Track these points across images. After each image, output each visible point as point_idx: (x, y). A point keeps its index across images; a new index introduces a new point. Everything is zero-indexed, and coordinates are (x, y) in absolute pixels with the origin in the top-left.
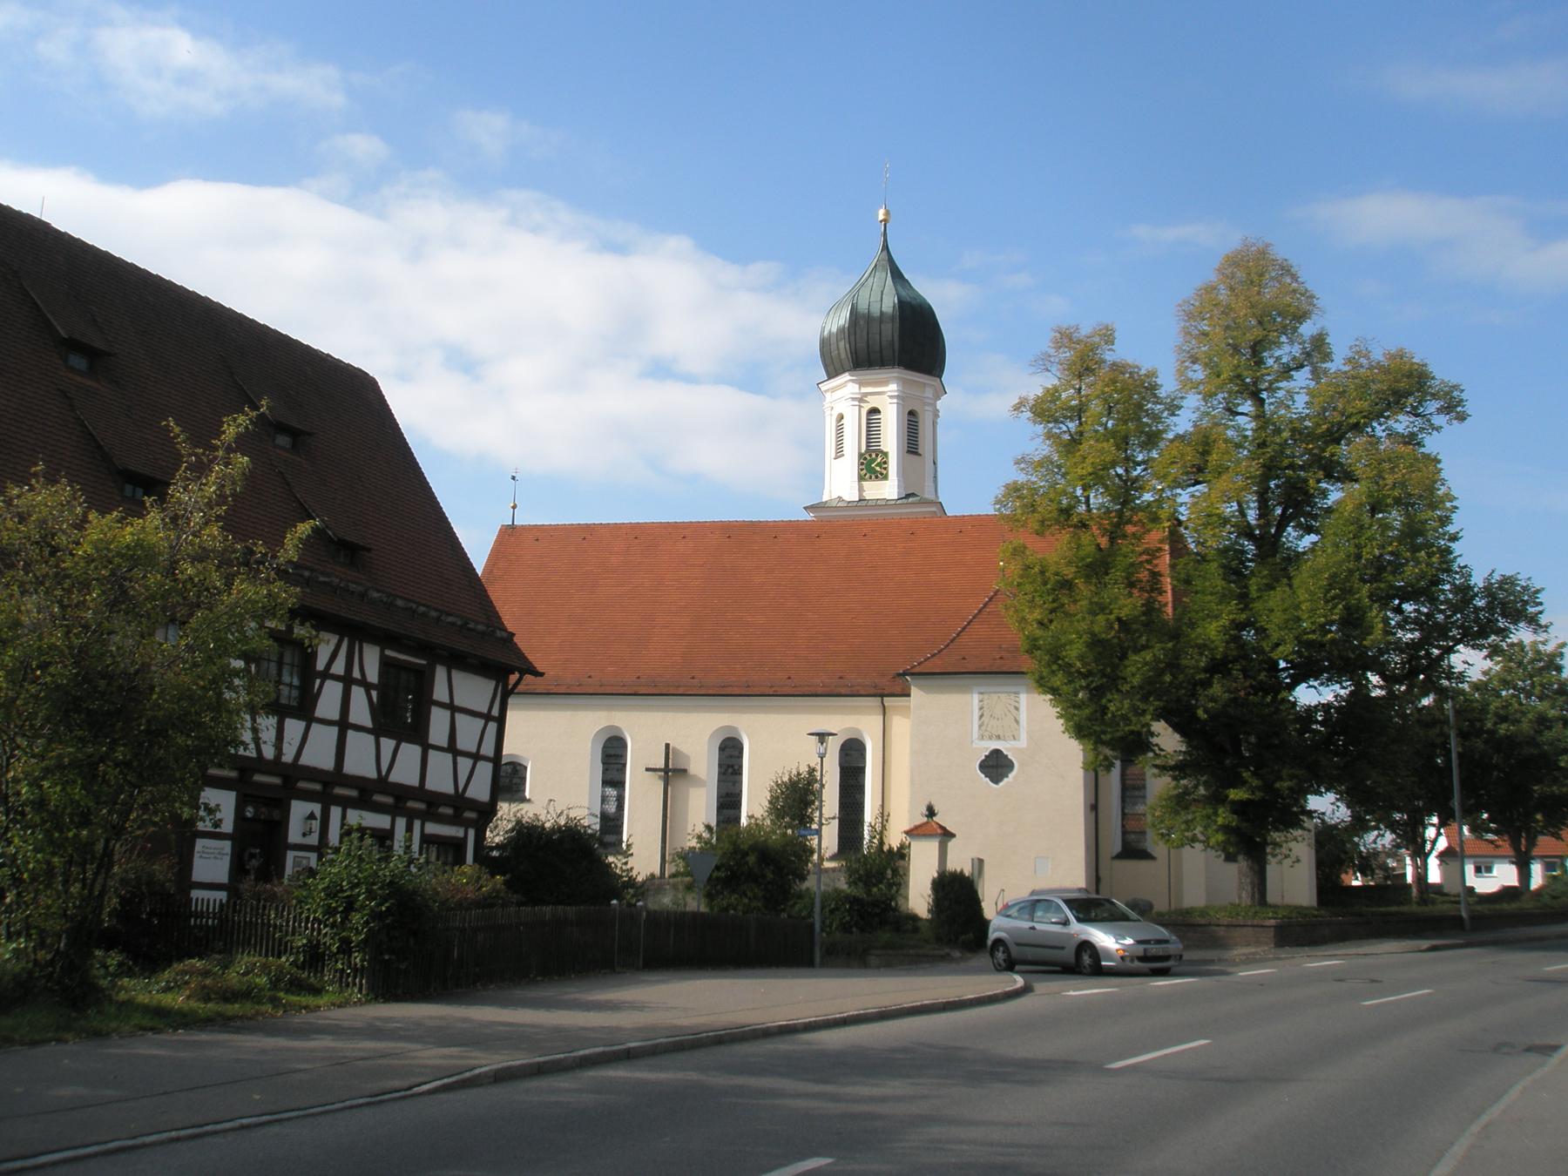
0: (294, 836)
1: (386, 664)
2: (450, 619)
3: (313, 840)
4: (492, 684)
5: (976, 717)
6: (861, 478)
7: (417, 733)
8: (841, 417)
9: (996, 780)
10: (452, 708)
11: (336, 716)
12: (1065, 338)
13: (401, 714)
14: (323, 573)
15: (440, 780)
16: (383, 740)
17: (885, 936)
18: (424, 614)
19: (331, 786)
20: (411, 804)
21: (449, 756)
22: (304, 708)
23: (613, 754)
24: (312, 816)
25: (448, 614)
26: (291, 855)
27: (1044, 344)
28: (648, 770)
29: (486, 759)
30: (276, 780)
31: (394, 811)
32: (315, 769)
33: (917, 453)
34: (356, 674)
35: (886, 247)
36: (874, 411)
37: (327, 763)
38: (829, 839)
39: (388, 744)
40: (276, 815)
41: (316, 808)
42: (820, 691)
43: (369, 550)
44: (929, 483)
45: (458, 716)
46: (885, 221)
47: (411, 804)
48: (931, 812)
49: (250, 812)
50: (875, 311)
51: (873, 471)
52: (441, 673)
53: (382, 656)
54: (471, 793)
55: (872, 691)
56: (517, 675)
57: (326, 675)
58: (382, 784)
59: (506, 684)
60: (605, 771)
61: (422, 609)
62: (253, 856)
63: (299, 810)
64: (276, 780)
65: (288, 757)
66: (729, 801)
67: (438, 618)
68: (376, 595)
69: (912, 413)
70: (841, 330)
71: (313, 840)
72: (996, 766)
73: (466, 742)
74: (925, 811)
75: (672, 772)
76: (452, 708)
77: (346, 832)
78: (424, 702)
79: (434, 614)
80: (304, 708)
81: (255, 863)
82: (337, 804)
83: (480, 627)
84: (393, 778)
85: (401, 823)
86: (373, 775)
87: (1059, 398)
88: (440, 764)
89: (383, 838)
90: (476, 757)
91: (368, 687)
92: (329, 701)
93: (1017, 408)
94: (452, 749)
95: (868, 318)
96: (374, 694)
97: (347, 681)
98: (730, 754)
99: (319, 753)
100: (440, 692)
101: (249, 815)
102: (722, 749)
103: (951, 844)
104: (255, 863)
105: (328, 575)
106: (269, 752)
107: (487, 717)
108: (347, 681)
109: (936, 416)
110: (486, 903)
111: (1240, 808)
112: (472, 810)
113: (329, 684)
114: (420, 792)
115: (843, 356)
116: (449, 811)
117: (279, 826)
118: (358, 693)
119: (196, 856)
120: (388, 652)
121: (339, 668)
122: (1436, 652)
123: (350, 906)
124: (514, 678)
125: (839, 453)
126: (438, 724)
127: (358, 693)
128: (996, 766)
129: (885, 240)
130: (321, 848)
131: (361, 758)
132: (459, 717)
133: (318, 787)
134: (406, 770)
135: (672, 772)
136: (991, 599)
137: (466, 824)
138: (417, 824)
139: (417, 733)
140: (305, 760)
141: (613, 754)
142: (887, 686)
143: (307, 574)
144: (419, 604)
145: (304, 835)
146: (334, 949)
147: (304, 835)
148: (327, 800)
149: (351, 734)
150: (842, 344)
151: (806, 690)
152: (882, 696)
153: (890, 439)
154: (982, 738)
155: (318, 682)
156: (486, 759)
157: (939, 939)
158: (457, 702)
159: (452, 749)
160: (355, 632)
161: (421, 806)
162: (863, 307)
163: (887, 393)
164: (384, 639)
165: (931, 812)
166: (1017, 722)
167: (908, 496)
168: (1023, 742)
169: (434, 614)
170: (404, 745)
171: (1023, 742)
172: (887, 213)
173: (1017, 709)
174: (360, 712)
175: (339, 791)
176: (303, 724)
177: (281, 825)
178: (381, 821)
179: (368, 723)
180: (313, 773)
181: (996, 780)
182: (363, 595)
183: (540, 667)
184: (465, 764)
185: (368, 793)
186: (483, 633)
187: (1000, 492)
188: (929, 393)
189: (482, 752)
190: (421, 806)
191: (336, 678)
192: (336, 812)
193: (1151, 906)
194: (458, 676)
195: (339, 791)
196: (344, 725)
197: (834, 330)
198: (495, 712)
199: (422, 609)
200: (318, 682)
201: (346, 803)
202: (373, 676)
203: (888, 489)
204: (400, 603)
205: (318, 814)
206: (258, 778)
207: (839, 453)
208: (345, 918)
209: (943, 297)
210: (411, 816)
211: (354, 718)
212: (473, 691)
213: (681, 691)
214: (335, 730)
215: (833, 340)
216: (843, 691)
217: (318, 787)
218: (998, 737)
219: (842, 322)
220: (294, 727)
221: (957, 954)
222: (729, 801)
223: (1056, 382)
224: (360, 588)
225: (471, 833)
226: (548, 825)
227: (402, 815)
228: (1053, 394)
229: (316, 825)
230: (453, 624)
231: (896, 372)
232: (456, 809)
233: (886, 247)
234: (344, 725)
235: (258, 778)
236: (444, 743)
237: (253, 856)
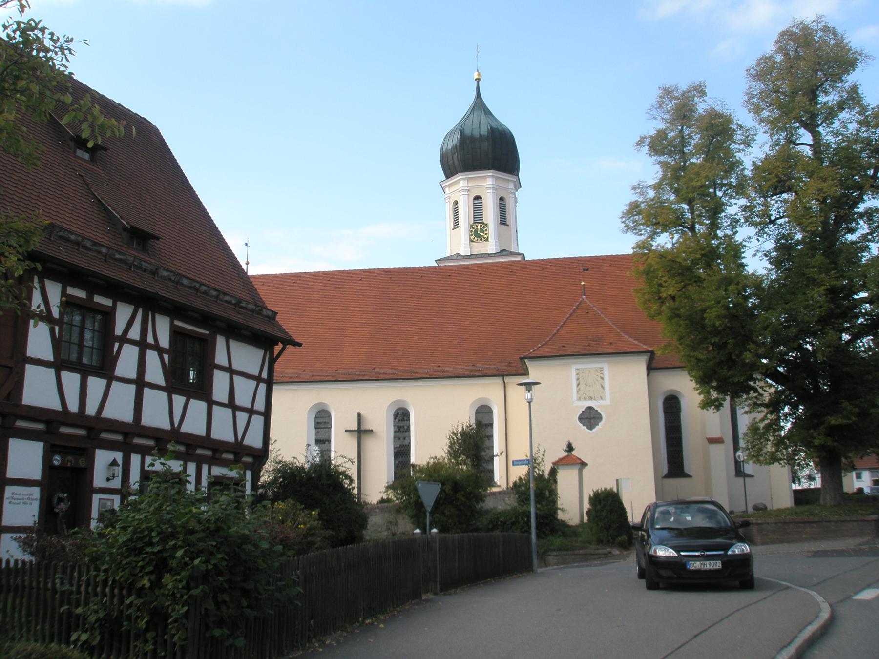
0: (99, 480)
1: (176, 334)
2: (227, 298)
3: (116, 484)
4: (262, 352)
5: (575, 383)
6: (472, 241)
7: (202, 390)
8: (456, 203)
9: (591, 428)
10: (231, 371)
11: (133, 375)
12: (667, 93)
13: (189, 372)
14: (119, 252)
15: (222, 431)
16: (175, 397)
17: (557, 541)
18: (205, 293)
19: (130, 437)
20: (199, 451)
21: (230, 411)
22: (105, 368)
23: (322, 420)
24: (114, 463)
25: (225, 294)
26: (96, 498)
27: (653, 96)
28: (346, 431)
29: (258, 413)
30: (82, 432)
31: (185, 457)
32: (116, 421)
33: (505, 224)
34: (150, 340)
35: (479, 95)
36: (478, 198)
37: (127, 416)
38: (248, 491)
39: (179, 400)
40: (82, 463)
41: (118, 456)
42: (461, 374)
43: (158, 238)
44: (514, 243)
45: (235, 377)
46: (478, 80)
47: (199, 451)
48: (570, 448)
49: (57, 460)
50: (476, 134)
51: (479, 236)
52: (220, 342)
53: (172, 325)
54: (247, 441)
55: (496, 373)
56: (280, 346)
57: (124, 339)
58: (175, 434)
59: (272, 353)
60: (317, 433)
61: (205, 288)
62: (61, 500)
63: (103, 458)
64: (82, 432)
65: (91, 410)
66: (402, 453)
67: (217, 297)
68: (165, 274)
69: (501, 199)
70: (454, 148)
71: (116, 484)
72: (590, 418)
73: (243, 398)
74: (565, 447)
75: (361, 432)
76: (231, 371)
77: (146, 476)
78: (206, 368)
79: (214, 293)
80: (105, 368)
81: (63, 506)
82: (136, 452)
83: (250, 306)
84: (184, 429)
85: (192, 468)
86: (168, 427)
87: (666, 138)
88: (222, 415)
89: (179, 480)
90: (251, 411)
91: (160, 351)
92: (127, 362)
93: (640, 143)
94: (231, 404)
95: (472, 139)
96: (166, 357)
97: (143, 345)
98: (402, 417)
99: (120, 407)
100: (221, 358)
101: (56, 463)
102: (396, 415)
103: (585, 470)
104: (63, 506)
105: (123, 254)
106: (73, 406)
107: (258, 379)
108: (142, 346)
109: (516, 202)
110: (305, 545)
111: (832, 431)
112: (248, 455)
113: (126, 347)
114: (206, 441)
115: (456, 163)
116: (231, 457)
117: (85, 472)
118: (152, 357)
119: (6, 502)
120: (177, 323)
121: (135, 333)
122: (846, 337)
123: (161, 565)
124: (278, 348)
125: (456, 225)
126: (220, 383)
127: (152, 357)
128: (590, 418)
129: (478, 88)
130: (123, 492)
131: (157, 412)
132: (236, 378)
133: (119, 438)
134: (194, 421)
135: (361, 432)
136: (577, 307)
137: (247, 466)
138: (205, 468)
139: (202, 390)
140: (107, 413)
141: (322, 420)
142: (510, 366)
143: (104, 251)
144: (202, 284)
145: (108, 480)
146: (142, 624)
147: (108, 480)
148: (127, 449)
149: (147, 391)
150: (455, 156)
151: (451, 374)
152: (503, 376)
153: (490, 214)
154: (579, 399)
155: (117, 345)
156: (258, 413)
157: (600, 541)
158: (235, 366)
159: (231, 404)
160: (149, 303)
161: (208, 453)
162: (468, 132)
163: (487, 183)
164: (174, 310)
165: (570, 448)
166: (603, 387)
167: (502, 251)
168: (607, 401)
169: (214, 293)
170: (193, 402)
171: (607, 401)
172: (479, 74)
173: (602, 378)
174: (155, 372)
175: (138, 441)
176: (103, 382)
177: (88, 471)
178: (176, 466)
179: (162, 383)
180: (114, 426)
181: (591, 428)
182: (154, 273)
183: (297, 340)
184: (242, 417)
185: (165, 441)
186: (253, 311)
187: (625, 209)
188: (511, 186)
189: (256, 407)
190: (208, 453)
191: (132, 342)
192: (135, 459)
193: (766, 508)
194: (234, 345)
195: (138, 441)
196: (140, 383)
197: (450, 147)
198: (265, 375)
199: (204, 288)
200: (117, 345)
201: (144, 451)
202: (165, 342)
203: (491, 247)
204: (185, 281)
205: (120, 461)
206: (64, 430)
207: (456, 225)
208: (157, 584)
209: (507, 116)
210: (200, 461)
211: (148, 378)
212: (247, 358)
213: (367, 377)
214: (133, 387)
215: (449, 154)
216: (477, 374)
217: (119, 438)
218: (591, 398)
219: (455, 142)
220: (96, 385)
221: (616, 552)
222: (402, 453)
223: (662, 126)
224: (151, 267)
225: (249, 474)
226: (307, 466)
227: (192, 461)
228: (661, 135)
229: (119, 470)
230: (229, 302)
231: (490, 173)
232: (236, 454)
233: (479, 95)
234: (140, 383)
235: (64, 430)
236: (225, 399)
237: (61, 500)
